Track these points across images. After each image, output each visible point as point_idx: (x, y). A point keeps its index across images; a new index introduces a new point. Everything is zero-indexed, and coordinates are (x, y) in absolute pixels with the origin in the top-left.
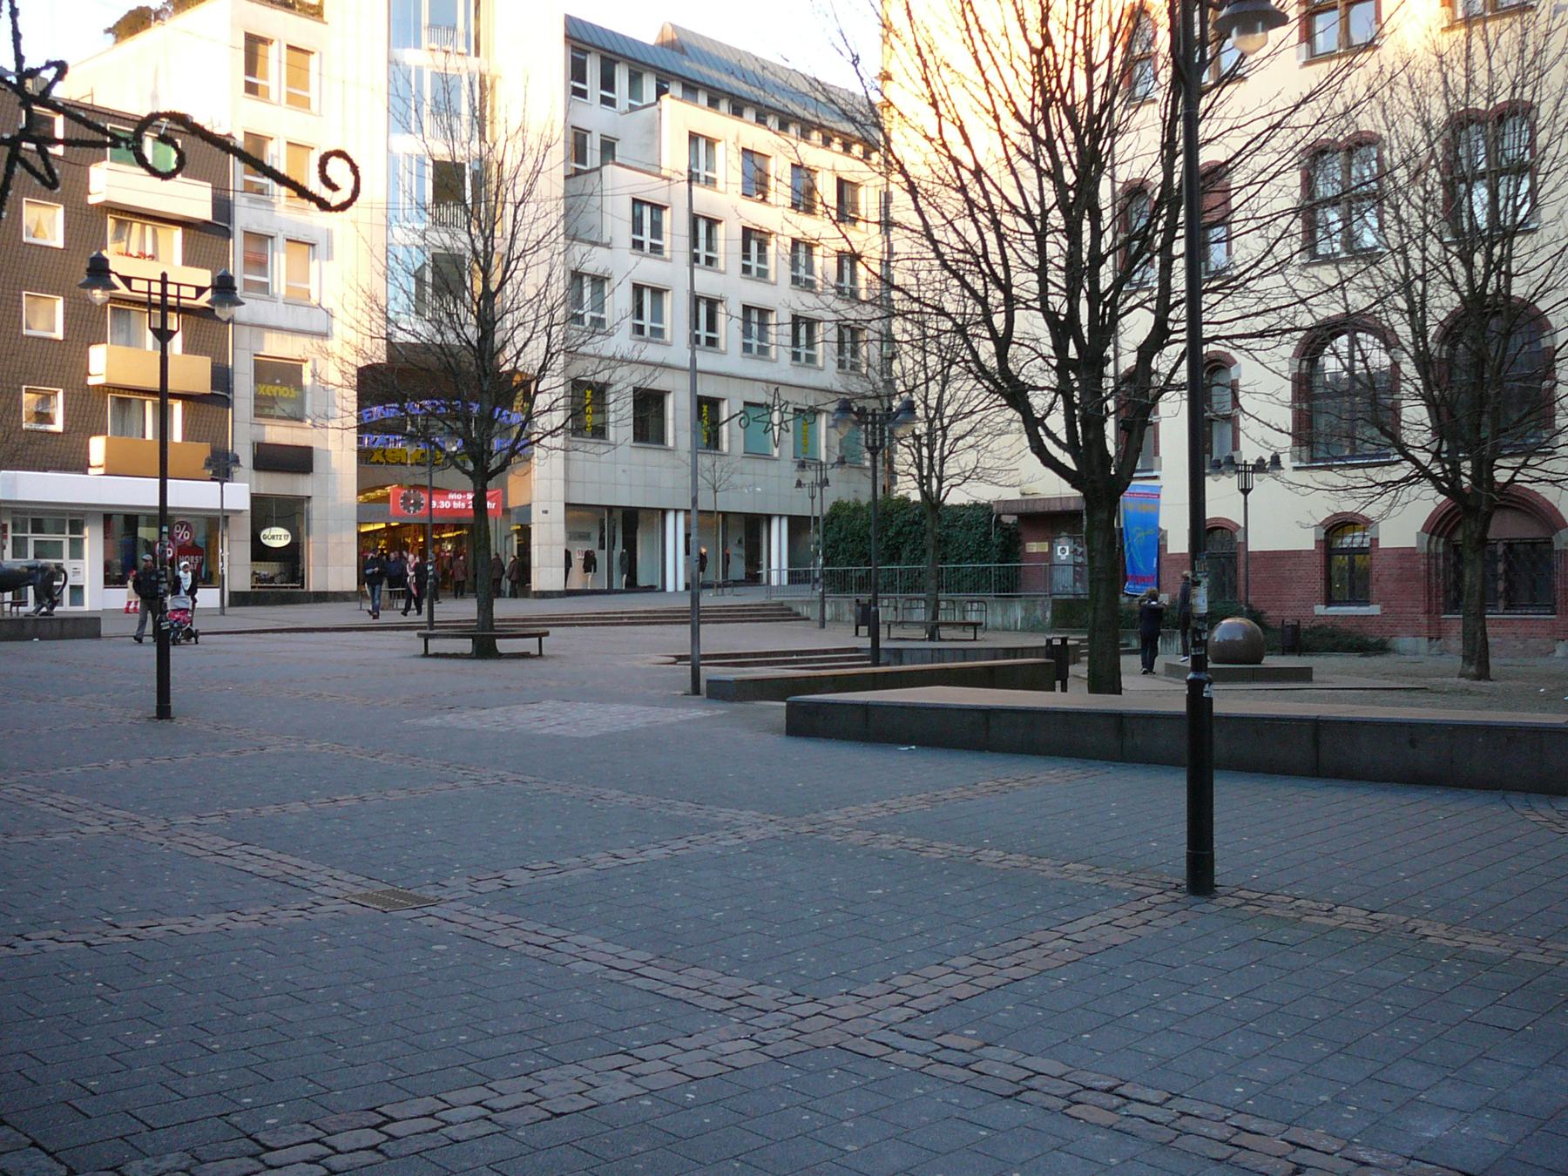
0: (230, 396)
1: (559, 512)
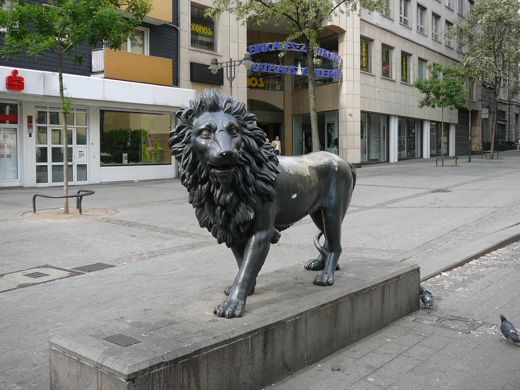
0: (178, 28)
1: (357, 117)
